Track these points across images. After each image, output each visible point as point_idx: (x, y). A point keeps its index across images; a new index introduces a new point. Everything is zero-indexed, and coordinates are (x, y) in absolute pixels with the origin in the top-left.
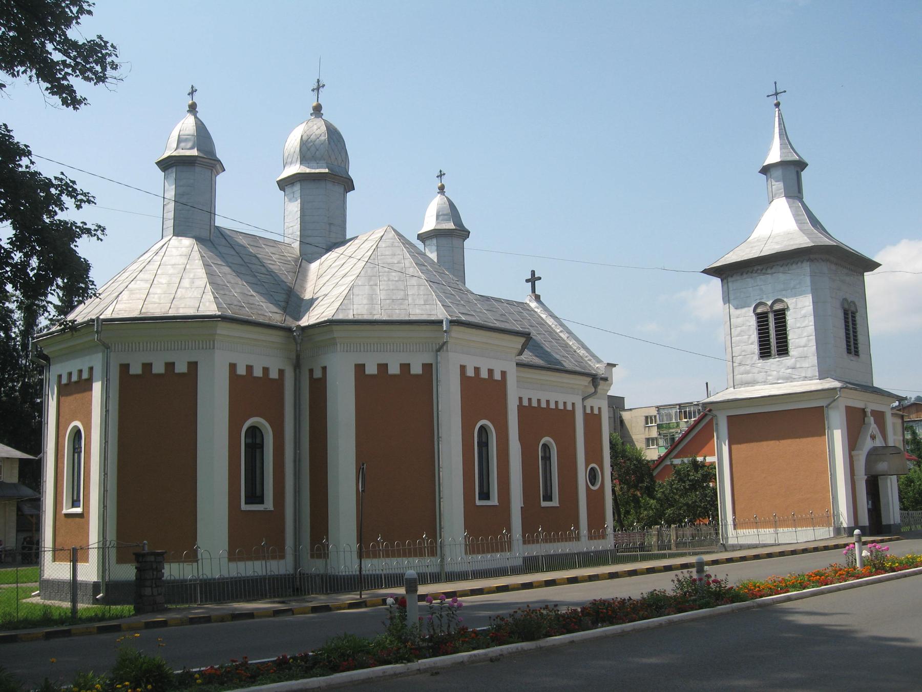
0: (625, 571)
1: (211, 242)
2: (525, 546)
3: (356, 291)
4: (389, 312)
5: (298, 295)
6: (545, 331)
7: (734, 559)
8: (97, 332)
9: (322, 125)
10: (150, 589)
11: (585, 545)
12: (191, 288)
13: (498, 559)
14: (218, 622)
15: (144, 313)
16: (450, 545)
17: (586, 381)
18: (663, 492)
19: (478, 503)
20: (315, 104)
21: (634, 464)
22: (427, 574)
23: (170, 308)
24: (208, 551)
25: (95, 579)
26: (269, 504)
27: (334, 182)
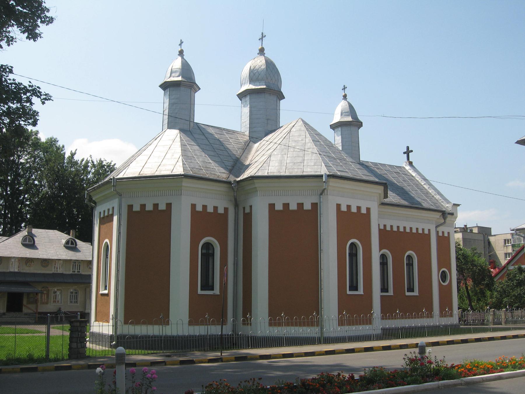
0: (430, 342)
1: (190, 131)
2: (384, 321)
3: (272, 158)
4: (291, 170)
5: (242, 162)
6: (414, 184)
7: (519, 336)
8: (113, 186)
9: (263, 60)
10: (76, 344)
11: (437, 320)
12: (171, 159)
13: (367, 330)
14: (109, 368)
15: (141, 174)
16: (333, 320)
17: (438, 215)
18: (502, 287)
19: (349, 292)
20: (260, 47)
21: (479, 269)
22: (316, 337)
23: (156, 171)
24: (181, 320)
25: (111, 333)
26: (217, 291)
27: (270, 94)
